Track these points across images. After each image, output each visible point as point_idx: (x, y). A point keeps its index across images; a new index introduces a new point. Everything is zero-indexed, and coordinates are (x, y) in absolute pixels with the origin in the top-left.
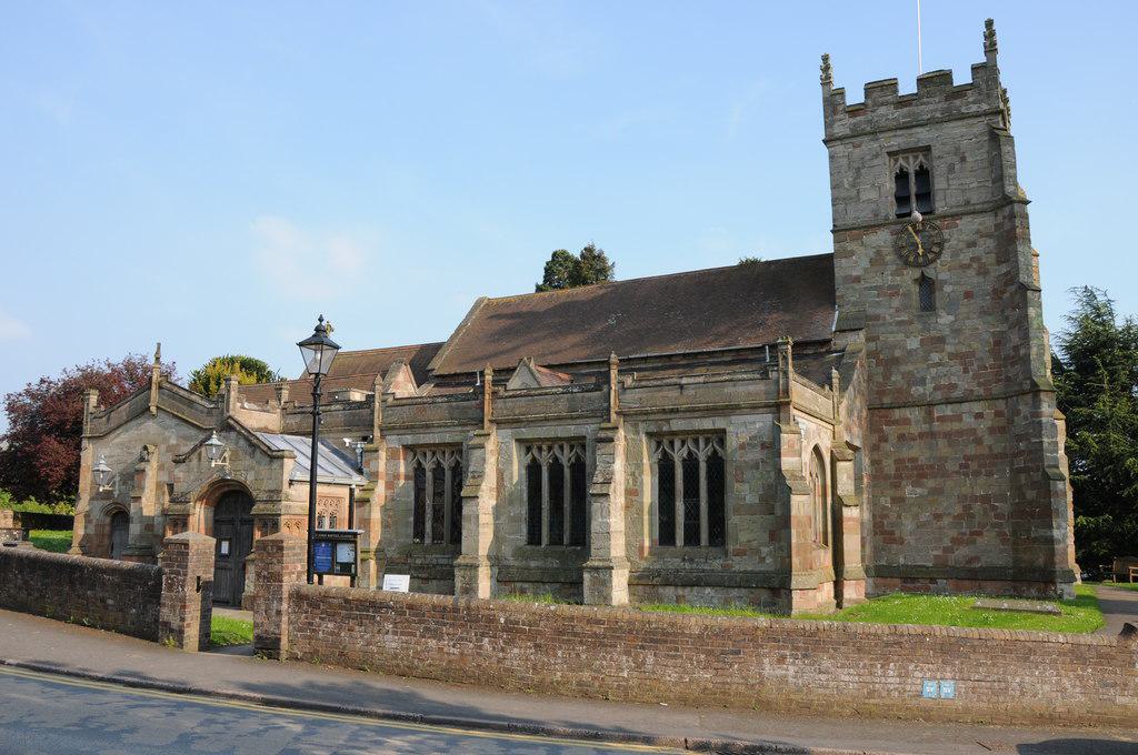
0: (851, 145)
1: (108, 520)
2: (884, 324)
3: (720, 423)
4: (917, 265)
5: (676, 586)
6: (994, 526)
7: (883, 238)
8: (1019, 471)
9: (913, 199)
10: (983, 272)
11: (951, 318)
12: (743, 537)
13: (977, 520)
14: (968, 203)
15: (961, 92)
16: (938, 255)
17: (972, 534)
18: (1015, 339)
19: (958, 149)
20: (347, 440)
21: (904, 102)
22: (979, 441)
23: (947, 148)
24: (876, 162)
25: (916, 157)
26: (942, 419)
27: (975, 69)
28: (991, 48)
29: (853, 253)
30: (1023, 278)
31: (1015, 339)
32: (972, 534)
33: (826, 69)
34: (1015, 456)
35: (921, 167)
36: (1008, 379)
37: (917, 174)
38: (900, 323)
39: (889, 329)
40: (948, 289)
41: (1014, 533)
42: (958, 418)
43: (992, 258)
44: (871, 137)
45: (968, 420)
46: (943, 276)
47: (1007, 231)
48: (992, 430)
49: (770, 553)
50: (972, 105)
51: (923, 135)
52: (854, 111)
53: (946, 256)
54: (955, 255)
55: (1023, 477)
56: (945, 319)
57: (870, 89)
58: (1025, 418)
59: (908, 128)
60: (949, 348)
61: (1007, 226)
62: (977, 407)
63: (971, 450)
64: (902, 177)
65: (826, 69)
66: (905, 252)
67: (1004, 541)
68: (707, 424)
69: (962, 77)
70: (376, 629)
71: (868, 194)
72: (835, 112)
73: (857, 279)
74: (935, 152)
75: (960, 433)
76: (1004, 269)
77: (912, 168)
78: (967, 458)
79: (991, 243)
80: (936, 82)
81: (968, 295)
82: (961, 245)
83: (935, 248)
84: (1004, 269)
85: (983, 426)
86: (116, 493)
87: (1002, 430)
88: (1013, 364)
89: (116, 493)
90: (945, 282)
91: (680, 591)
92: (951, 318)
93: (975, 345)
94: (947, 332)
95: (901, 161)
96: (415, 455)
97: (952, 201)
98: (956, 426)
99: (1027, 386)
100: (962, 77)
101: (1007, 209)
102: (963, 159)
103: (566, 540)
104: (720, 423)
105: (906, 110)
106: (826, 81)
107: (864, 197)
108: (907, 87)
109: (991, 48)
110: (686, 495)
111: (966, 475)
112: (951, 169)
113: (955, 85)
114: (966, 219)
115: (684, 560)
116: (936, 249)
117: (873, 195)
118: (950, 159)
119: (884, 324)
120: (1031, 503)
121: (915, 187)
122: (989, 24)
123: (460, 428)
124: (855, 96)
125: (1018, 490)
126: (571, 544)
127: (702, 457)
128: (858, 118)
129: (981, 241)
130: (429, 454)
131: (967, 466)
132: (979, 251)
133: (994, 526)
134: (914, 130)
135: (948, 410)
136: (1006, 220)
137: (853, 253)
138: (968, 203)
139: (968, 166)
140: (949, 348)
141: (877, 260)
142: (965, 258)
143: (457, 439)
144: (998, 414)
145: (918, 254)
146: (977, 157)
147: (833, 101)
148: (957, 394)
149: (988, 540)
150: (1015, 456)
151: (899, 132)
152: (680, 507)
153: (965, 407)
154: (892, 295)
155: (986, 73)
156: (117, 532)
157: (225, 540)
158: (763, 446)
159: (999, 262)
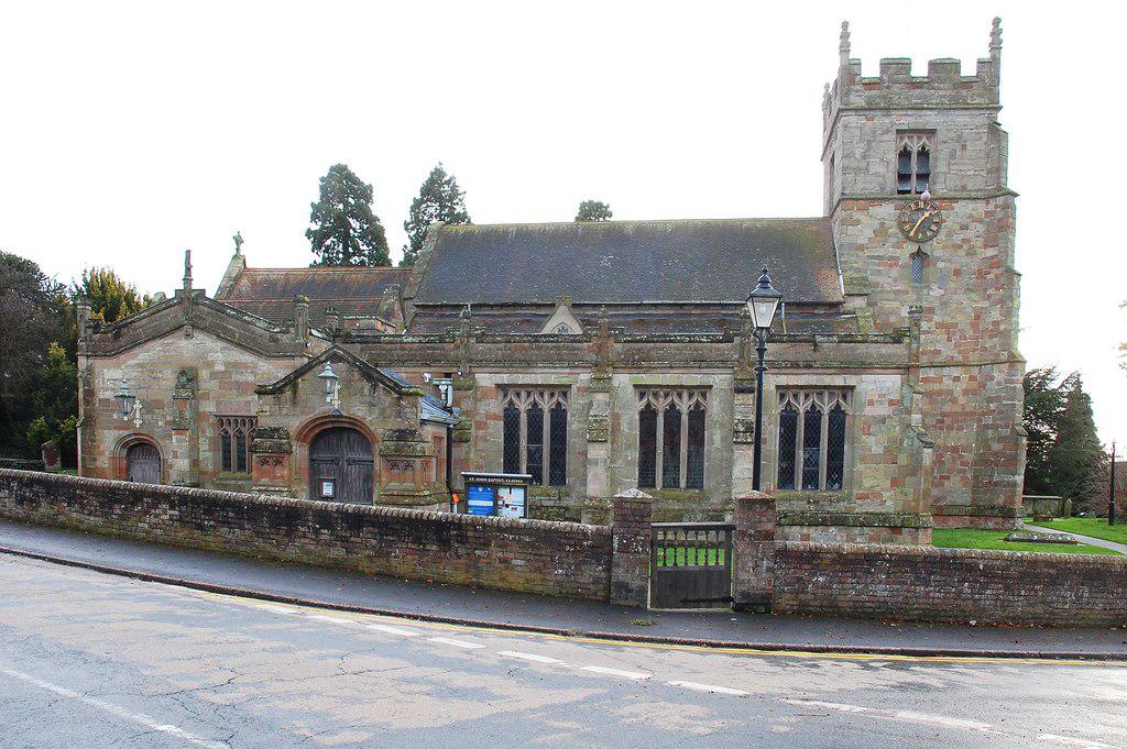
0: (863, 117)
1: (125, 452)
2: (882, 292)
3: (851, 380)
4: (915, 240)
5: (802, 525)
6: (959, 471)
7: (887, 211)
8: (987, 427)
9: (914, 178)
10: (971, 253)
11: (942, 292)
12: (867, 483)
13: (947, 466)
14: (964, 188)
15: (968, 84)
16: (936, 233)
17: (942, 477)
18: (996, 314)
19: (960, 137)
20: (428, 376)
21: (916, 84)
22: (954, 401)
23: (952, 135)
24: (886, 137)
25: (919, 138)
26: (925, 380)
27: (980, 62)
28: (996, 46)
29: (858, 222)
30: (1009, 263)
31: (996, 314)
32: (942, 477)
33: (845, 36)
34: (983, 414)
35: (923, 148)
36: (984, 349)
37: (919, 154)
38: (897, 292)
39: (886, 296)
40: (941, 265)
41: (976, 477)
42: (939, 380)
43: (979, 242)
44: (885, 112)
45: (948, 383)
46: (938, 253)
47: (999, 220)
48: (965, 392)
49: (890, 498)
50: (971, 91)
51: (931, 119)
52: (871, 84)
53: (942, 236)
54: (949, 235)
55: (990, 432)
56: (936, 292)
57: (886, 65)
58: (999, 383)
59: (918, 109)
60: (937, 319)
61: (999, 215)
62: (956, 372)
63: (948, 408)
64: (905, 155)
65: (845, 36)
66: (907, 227)
67: (965, 484)
68: (838, 381)
69: (969, 70)
70: (869, 580)
71: (876, 168)
72: (852, 82)
73: (861, 248)
74: (940, 136)
75: (940, 393)
76: (990, 252)
77: (915, 147)
78: (944, 415)
79: (981, 228)
80: (944, 69)
81: (957, 273)
82: (957, 227)
83: (929, 229)
84: (990, 252)
85: (958, 388)
86: (138, 423)
87: (974, 393)
88: (991, 337)
89: (138, 423)
90: (939, 259)
91: (805, 530)
92: (942, 292)
93: (959, 318)
94: (936, 304)
95: (906, 140)
96: (505, 396)
97: (951, 184)
98: (936, 387)
99: (1004, 356)
100: (969, 70)
101: (1000, 200)
102: (964, 147)
103: (683, 483)
104: (851, 380)
105: (917, 91)
106: (845, 48)
107: (874, 169)
108: (920, 70)
109: (996, 46)
110: (807, 443)
111: (941, 429)
112: (952, 155)
113: (962, 74)
114: (961, 203)
115: (809, 502)
116: (934, 228)
117: (881, 170)
118: (952, 145)
119: (882, 292)
120: (996, 454)
121: (914, 167)
122: (997, 22)
123: (568, 371)
124: (871, 70)
125: (985, 443)
126: (688, 487)
127: (826, 410)
128: (874, 92)
129: (972, 226)
130: (523, 394)
131: (942, 422)
132: (969, 234)
133: (959, 471)
134: (923, 113)
135: (932, 373)
136: (998, 210)
137: (858, 222)
138: (964, 188)
139: (967, 154)
140: (937, 319)
141: (881, 231)
142: (957, 239)
143: (565, 381)
144: (972, 378)
145: (919, 234)
146: (977, 146)
147: (850, 71)
148: (940, 359)
149: (954, 483)
150: (983, 414)
151: (910, 112)
152: (800, 455)
153: (946, 371)
154: (891, 265)
155: (990, 68)
156: (137, 467)
157: (326, 480)
158: (891, 403)
159: (986, 246)
